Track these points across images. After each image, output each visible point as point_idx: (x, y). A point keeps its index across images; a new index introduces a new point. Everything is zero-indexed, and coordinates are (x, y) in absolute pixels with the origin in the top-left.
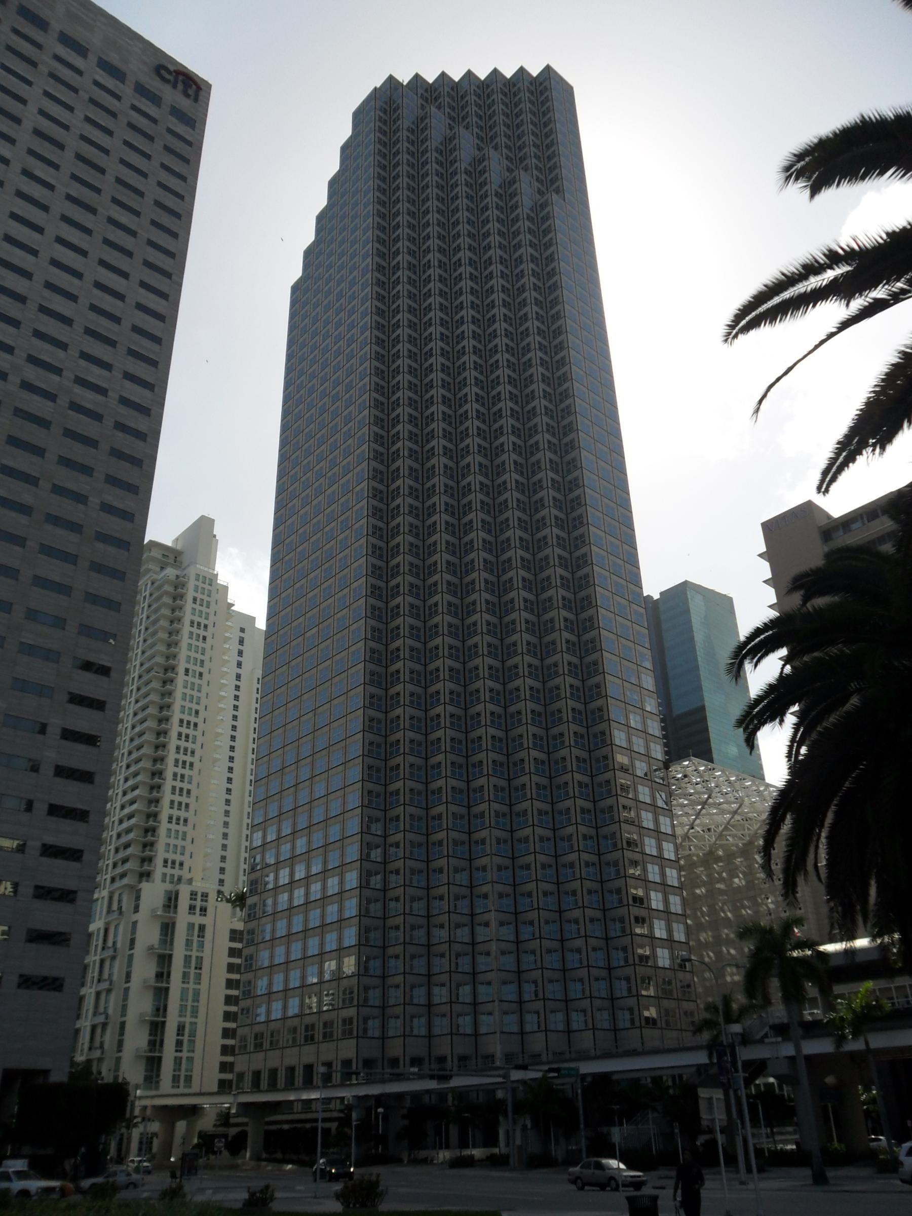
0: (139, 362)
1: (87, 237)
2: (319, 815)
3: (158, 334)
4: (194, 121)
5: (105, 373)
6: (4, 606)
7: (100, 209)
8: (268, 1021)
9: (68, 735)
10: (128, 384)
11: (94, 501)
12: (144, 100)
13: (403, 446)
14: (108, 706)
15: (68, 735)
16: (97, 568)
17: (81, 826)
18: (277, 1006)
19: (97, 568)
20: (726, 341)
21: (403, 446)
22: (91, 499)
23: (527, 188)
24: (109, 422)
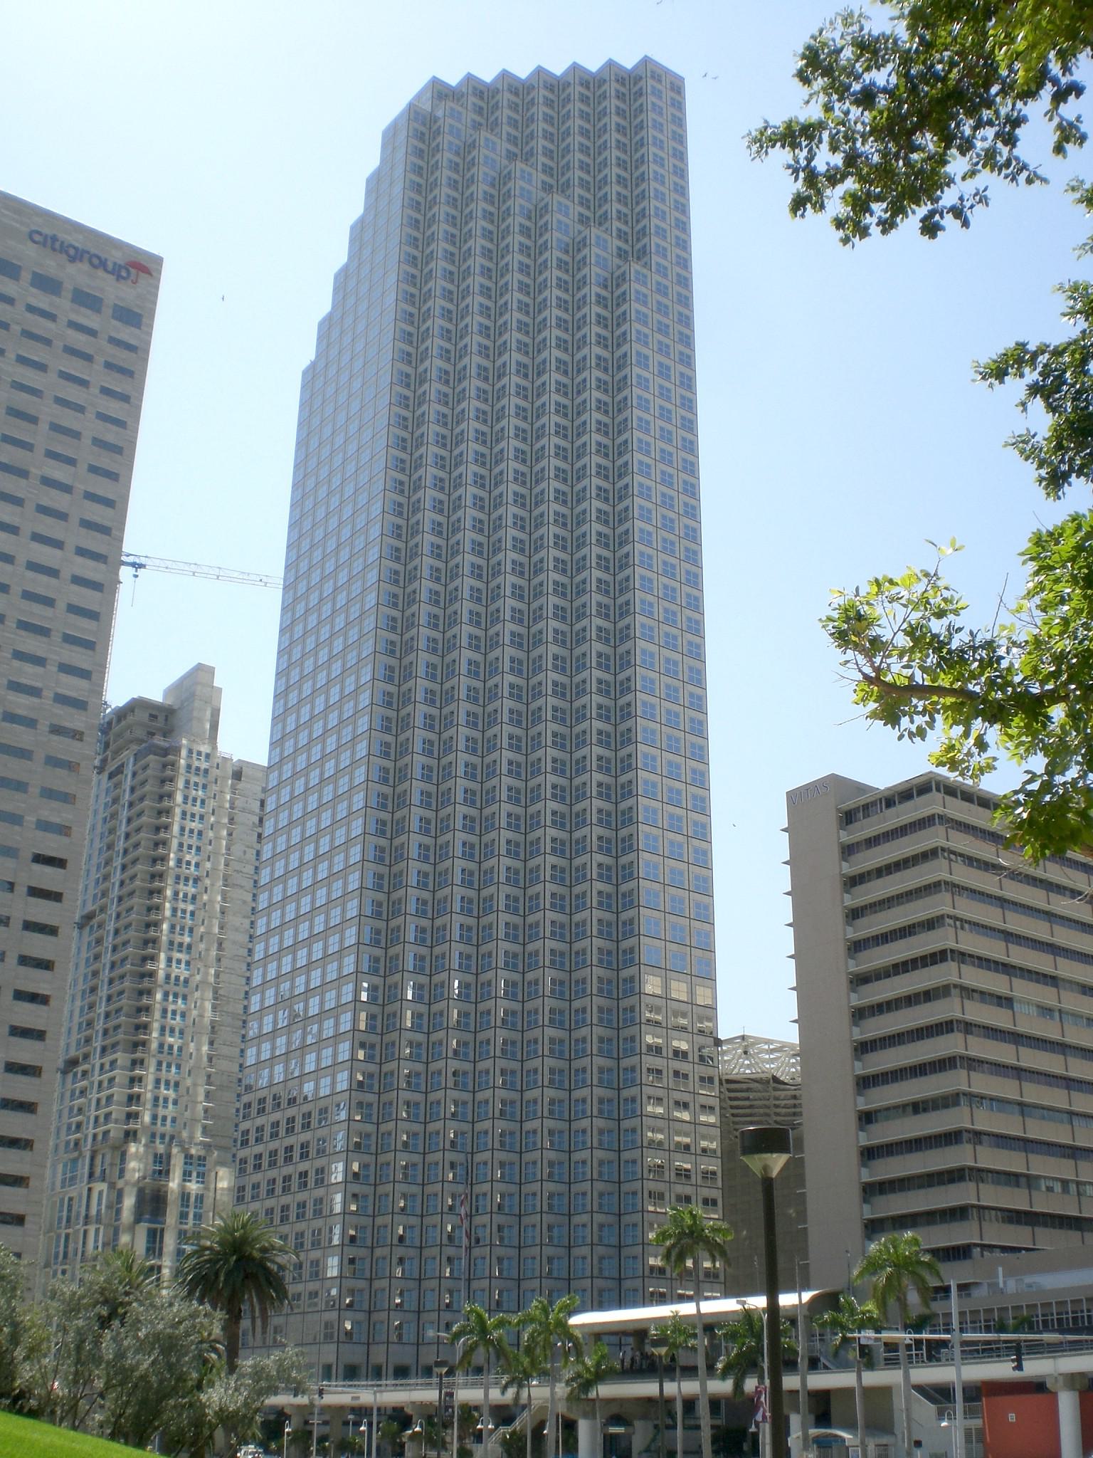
0: (74, 648)
1: (18, 509)
2: (325, 845)
3: (95, 608)
4: (137, 318)
5: (39, 670)
6: (1, 588)
7: (33, 470)
8: (271, 1085)
9: (35, 892)
10: (65, 678)
11: (30, 819)
12: (83, 309)
13: (439, 284)
14: (48, 1035)
15: (35, 892)
16: (66, 669)
17: (26, 1154)
18: (279, 1069)
19: (66, 669)
20: (997, 372)
21: (439, 284)
22: (27, 818)
23: (602, 248)
24: (43, 726)
